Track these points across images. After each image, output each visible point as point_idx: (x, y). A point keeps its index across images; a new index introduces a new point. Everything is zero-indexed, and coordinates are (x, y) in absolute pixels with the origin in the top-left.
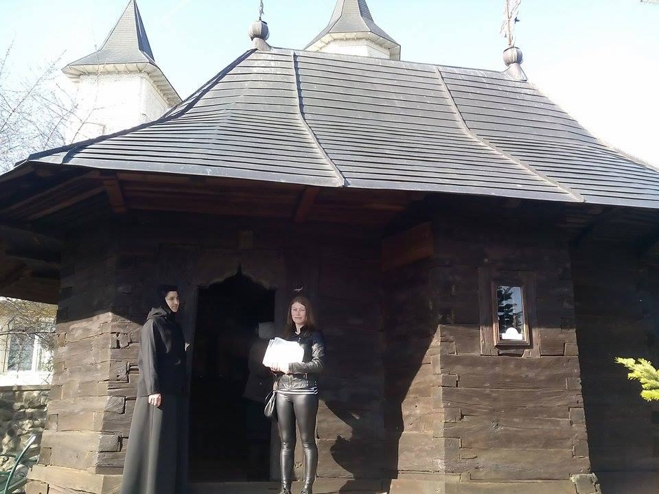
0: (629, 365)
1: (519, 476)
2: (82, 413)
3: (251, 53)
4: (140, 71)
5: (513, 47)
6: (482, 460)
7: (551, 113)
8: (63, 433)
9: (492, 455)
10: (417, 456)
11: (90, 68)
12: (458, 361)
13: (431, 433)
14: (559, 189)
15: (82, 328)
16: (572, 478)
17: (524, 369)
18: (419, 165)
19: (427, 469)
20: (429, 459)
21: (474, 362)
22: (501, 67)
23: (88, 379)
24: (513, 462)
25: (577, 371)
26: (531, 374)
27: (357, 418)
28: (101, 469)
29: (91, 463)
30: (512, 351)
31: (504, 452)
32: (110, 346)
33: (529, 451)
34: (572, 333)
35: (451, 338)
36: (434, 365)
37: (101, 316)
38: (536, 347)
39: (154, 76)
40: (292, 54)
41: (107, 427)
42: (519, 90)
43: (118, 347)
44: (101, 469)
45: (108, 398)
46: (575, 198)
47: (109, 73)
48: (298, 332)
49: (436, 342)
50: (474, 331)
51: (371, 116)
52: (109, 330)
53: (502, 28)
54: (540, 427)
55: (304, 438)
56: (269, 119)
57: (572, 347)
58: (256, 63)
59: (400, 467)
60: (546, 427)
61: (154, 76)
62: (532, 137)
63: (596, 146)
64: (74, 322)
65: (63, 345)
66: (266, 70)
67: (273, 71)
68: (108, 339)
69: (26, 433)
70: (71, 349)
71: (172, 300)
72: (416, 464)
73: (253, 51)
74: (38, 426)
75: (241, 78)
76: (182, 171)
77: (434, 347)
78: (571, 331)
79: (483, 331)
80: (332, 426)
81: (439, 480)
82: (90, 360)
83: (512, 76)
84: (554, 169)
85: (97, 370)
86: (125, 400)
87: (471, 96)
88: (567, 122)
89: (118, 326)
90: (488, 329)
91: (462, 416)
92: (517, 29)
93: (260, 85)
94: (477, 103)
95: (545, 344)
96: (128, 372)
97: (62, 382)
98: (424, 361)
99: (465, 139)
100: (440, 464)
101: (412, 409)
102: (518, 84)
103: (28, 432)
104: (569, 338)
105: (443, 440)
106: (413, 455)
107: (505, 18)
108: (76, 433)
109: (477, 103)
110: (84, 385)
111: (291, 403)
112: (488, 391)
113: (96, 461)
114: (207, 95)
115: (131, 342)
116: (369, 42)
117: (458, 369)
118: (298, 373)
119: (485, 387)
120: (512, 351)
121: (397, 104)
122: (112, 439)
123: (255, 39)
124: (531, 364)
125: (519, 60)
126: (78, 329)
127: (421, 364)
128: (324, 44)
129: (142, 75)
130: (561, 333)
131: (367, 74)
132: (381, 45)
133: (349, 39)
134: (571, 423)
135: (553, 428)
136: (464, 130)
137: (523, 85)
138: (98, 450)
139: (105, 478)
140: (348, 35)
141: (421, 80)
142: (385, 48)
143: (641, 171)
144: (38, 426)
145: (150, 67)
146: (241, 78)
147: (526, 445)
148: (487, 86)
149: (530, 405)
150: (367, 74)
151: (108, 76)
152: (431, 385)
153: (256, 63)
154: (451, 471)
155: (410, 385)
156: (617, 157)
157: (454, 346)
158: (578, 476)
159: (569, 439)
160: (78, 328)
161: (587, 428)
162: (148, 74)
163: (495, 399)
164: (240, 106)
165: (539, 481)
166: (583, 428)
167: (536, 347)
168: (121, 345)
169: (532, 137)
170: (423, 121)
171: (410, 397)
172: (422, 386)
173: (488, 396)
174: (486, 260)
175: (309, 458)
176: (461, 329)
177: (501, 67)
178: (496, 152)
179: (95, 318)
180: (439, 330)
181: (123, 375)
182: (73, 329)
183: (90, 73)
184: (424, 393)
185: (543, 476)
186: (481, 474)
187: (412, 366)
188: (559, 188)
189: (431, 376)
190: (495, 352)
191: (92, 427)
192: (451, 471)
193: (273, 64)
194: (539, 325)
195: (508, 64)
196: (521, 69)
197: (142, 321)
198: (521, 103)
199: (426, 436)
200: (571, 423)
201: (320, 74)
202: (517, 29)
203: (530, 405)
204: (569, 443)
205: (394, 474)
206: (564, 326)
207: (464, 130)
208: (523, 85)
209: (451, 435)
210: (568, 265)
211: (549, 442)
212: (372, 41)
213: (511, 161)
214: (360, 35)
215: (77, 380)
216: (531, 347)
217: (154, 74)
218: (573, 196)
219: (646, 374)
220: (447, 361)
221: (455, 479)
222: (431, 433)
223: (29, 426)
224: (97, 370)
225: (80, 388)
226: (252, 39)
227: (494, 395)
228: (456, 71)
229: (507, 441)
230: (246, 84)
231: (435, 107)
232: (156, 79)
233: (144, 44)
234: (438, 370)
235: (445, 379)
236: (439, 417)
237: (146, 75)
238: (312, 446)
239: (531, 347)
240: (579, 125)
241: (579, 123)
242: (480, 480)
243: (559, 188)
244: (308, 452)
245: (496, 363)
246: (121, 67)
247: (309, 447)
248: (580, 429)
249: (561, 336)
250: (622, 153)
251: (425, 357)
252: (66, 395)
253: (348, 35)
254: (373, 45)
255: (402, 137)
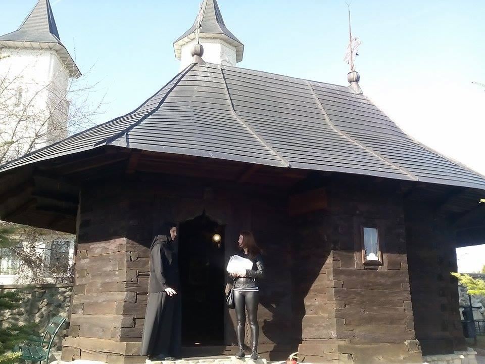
0: (458, 277)
1: (377, 341)
2: (104, 303)
3: (193, 66)
4: (51, 49)
5: (354, 71)
6: (357, 331)
7: (379, 117)
8: (88, 316)
9: (362, 328)
10: (317, 330)
11: (11, 43)
12: (342, 272)
13: (326, 315)
14: (401, 171)
15: (101, 247)
16: (406, 342)
17: (379, 277)
18: (320, 153)
19: (324, 337)
20: (325, 332)
21: (351, 273)
22: (347, 84)
23: (107, 280)
24: (373, 333)
25: (407, 279)
26: (383, 281)
27: (275, 307)
28: (123, 338)
29: (115, 335)
30: (372, 267)
31: (369, 327)
32: (126, 259)
33: (383, 326)
34: (405, 256)
35: (339, 258)
36: (329, 275)
37: (117, 239)
38: (385, 265)
39: (61, 54)
40: (220, 68)
41: (127, 311)
42: (359, 100)
43: (131, 260)
44: (123, 338)
45: (126, 293)
46: (413, 178)
47: (25, 48)
48: (246, 253)
49: (329, 261)
50: (351, 254)
51: (275, 114)
52: (125, 249)
53: (346, 58)
54: (388, 312)
55: (251, 318)
56: (215, 114)
57: (405, 265)
58: (198, 74)
59: (303, 336)
60: (392, 312)
61: (61, 54)
62: (371, 133)
63: (408, 140)
64: (93, 243)
65: (84, 258)
66: (205, 79)
67: (210, 79)
68: (124, 255)
69: (7, 319)
70: (92, 261)
71: (173, 233)
72: (316, 334)
73: (195, 64)
74: (15, 314)
75: (190, 83)
76: (197, 153)
77: (328, 264)
78: (404, 255)
79: (356, 255)
80: (265, 314)
81: (334, 343)
82: (109, 268)
83: (353, 90)
84: (391, 157)
85: (115, 275)
86: (137, 294)
87: (332, 103)
88: (394, 129)
89: (131, 247)
90: (359, 253)
91: (345, 305)
92: (356, 60)
93: (204, 89)
94: (336, 108)
95: (390, 264)
96: (137, 277)
97: (85, 283)
98: (321, 272)
99: (334, 134)
100: (334, 334)
101: (312, 302)
102: (357, 96)
103: (8, 319)
104: (403, 260)
105: (335, 320)
106: (314, 329)
107: (348, 51)
108: (101, 316)
109: (336, 108)
110: (104, 285)
111: (243, 296)
112: (359, 290)
113: (119, 333)
114: (170, 95)
115: (139, 258)
116: (222, 41)
117: (343, 277)
118: (249, 276)
119: (358, 288)
120: (372, 267)
121: (289, 106)
122: (130, 319)
123: (195, 56)
124: (382, 275)
125: (357, 80)
126: (97, 248)
127: (319, 274)
128: (190, 40)
129: (52, 52)
130: (400, 256)
131: (268, 85)
132: (230, 44)
133: (208, 38)
134: (405, 310)
135: (394, 313)
136: (331, 126)
137: (360, 97)
138: (121, 326)
139: (127, 344)
140: (208, 35)
141: (300, 90)
142: (233, 46)
143: (478, 177)
144: (15, 314)
145: (58, 47)
146: (190, 83)
147: (380, 323)
148: (340, 97)
149: (383, 299)
150: (268, 85)
151: (31, 51)
152: (326, 286)
153: (198, 74)
154: (340, 338)
155: (311, 287)
156: (422, 149)
157: (340, 263)
158: (409, 341)
159: (403, 319)
160: (98, 248)
161: (413, 313)
162: (57, 51)
163: (363, 296)
164: (195, 104)
165: (388, 344)
166: (411, 313)
167: (385, 265)
168: (132, 259)
169: (371, 133)
170: (307, 119)
171: (311, 294)
172: (319, 288)
173: (358, 294)
174: (358, 212)
175: (254, 331)
176: (344, 253)
177: (347, 84)
178: (356, 144)
179: (112, 241)
180: (331, 253)
181: (134, 279)
182: (94, 248)
183: (10, 47)
184: (321, 291)
185: (390, 342)
186: (357, 339)
187: (313, 275)
188: (401, 171)
189: (326, 281)
190: (363, 267)
191: (115, 312)
192: (340, 338)
193: (209, 74)
194: (387, 252)
195: (351, 82)
196: (358, 86)
197: (147, 242)
198: (361, 109)
199: (323, 317)
200: (405, 310)
201: (240, 83)
202: (356, 60)
203: (383, 299)
204: (403, 322)
205: (300, 341)
206: (400, 252)
207: (331, 126)
208: (360, 97)
209: (340, 316)
210: (403, 216)
211: (393, 321)
212: (225, 41)
213: (367, 150)
214: (216, 35)
215: (99, 281)
216: (382, 265)
217: (61, 52)
218: (412, 177)
219: (469, 281)
220: (337, 272)
221: (342, 343)
222: (326, 315)
223: (9, 314)
224: (115, 275)
225: (101, 286)
226: (193, 56)
227: (363, 293)
228: (320, 85)
229: (370, 320)
230: (195, 88)
231: (312, 110)
232: (62, 55)
233: (53, 29)
234: (331, 277)
235: (335, 283)
236: (333, 305)
237: (54, 52)
238: (256, 323)
239: (382, 265)
240: (389, 119)
241: (390, 118)
242: (357, 343)
243: (401, 171)
244: (253, 327)
245: (363, 274)
246: (36, 45)
247: (254, 324)
248: (410, 314)
249: (399, 258)
250: (424, 145)
251: (322, 269)
252: (89, 291)
253: (208, 35)
254: (225, 44)
255: (300, 131)
